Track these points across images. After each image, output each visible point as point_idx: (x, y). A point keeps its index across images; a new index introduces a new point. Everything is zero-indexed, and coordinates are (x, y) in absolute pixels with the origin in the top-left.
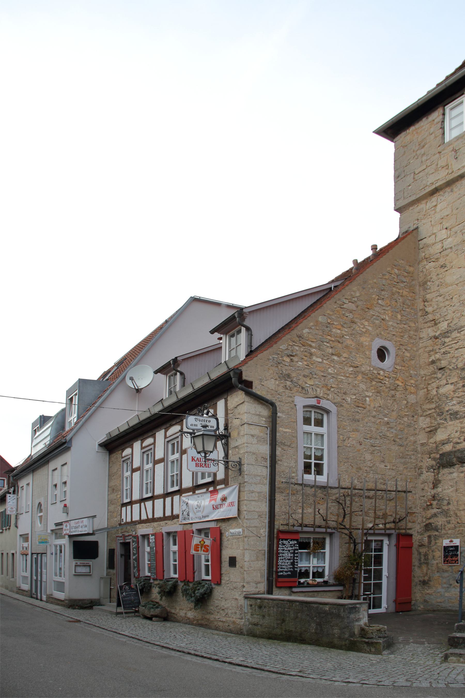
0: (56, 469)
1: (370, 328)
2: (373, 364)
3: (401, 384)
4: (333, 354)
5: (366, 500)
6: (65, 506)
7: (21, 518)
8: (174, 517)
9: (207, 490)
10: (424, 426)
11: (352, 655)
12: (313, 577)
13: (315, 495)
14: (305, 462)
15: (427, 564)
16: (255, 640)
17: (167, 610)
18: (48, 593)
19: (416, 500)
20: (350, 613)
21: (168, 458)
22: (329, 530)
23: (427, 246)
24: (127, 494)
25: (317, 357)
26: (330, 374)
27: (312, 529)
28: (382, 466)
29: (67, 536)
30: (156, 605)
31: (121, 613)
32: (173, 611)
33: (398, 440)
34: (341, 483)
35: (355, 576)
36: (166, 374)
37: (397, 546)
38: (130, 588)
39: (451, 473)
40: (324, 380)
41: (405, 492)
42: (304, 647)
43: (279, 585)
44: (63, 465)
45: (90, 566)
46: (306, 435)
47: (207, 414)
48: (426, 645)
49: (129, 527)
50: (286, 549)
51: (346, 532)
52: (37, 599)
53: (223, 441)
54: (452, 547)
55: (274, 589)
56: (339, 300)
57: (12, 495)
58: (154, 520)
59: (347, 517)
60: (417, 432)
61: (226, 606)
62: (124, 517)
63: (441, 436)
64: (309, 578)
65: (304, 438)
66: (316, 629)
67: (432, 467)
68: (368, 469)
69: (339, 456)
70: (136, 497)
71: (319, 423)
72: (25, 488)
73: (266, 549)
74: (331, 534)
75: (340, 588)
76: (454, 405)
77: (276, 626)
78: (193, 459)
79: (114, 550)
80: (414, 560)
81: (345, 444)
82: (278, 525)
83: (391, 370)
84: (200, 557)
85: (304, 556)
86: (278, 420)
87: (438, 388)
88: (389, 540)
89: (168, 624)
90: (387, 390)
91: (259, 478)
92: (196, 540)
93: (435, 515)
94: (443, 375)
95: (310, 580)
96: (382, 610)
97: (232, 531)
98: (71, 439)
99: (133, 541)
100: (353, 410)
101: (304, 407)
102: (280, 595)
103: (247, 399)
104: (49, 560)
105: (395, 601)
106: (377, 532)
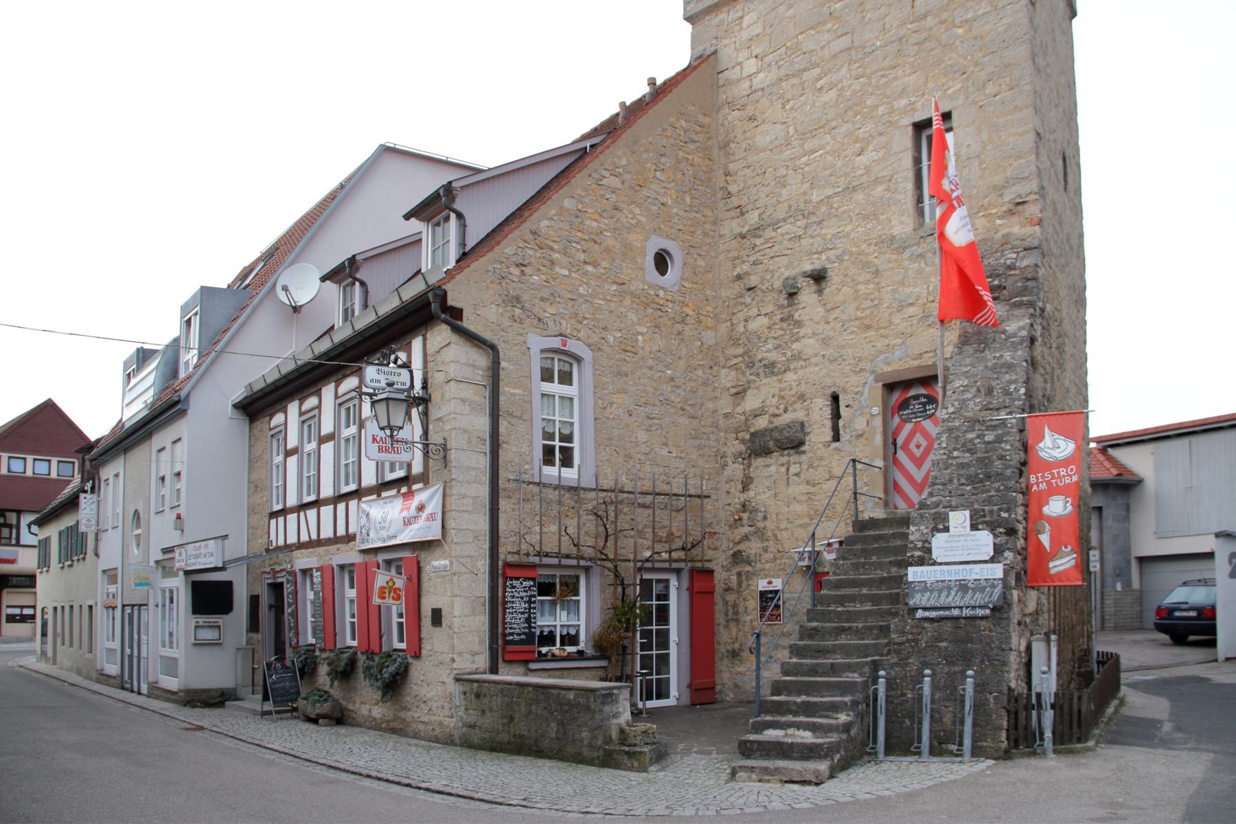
0: (163, 449)
1: (643, 219)
2: (648, 278)
3: (691, 313)
5: (640, 510)
6: (179, 517)
7: (104, 536)
8: (350, 538)
9: (399, 491)
10: (728, 385)
11: (607, 773)
12: (562, 644)
13: (560, 503)
14: (544, 446)
15: (737, 621)
16: (471, 752)
17: (341, 705)
18: (151, 679)
19: (718, 511)
20: (603, 703)
21: (331, 436)
22: (583, 563)
23: (730, 83)
24: (309, 485)
25: (562, 268)
27: (555, 561)
28: (664, 452)
29: (181, 573)
30: (325, 696)
31: (269, 713)
32: (350, 707)
33: (688, 408)
34: (600, 482)
35: (626, 642)
36: (339, 282)
37: (690, 589)
38: (284, 666)
40: (573, 306)
41: (699, 497)
42: (540, 762)
43: (507, 657)
44: (174, 442)
47: (395, 362)
48: (714, 755)
49: (281, 556)
50: (518, 593)
51: (610, 565)
52: (132, 691)
53: (420, 408)
54: (771, 592)
55: (501, 665)
56: (596, 171)
57: (88, 496)
58: (319, 543)
59: (611, 539)
60: (718, 394)
61: (428, 696)
62: (273, 537)
63: (751, 402)
64: (554, 645)
65: (546, 405)
66: (558, 731)
67: (741, 454)
68: (643, 458)
69: (596, 436)
70: (292, 501)
71: (566, 378)
72: (111, 481)
73: (487, 594)
74: (587, 569)
75: (603, 663)
77: (500, 727)
78: (374, 440)
79: (258, 597)
80: (717, 615)
81: (606, 414)
82: (506, 551)
83: (675, 289)
84: (389, 609)
85: (547, 607)
87: (746, 321)
88: (679, 580)
89: (343, 730)
90: (669, 323)
91: (473, 473)
92: (381, 579)
93: (746, 538)
94: (753, 299)
95: (556, 650)
96: (670, 702)
97: (435, 563)
98: (188, 395)
99: (288, 582)
100: (618, 356)
101: (542, 351)
102: (511, 675)
103: (454, 338)
104: (151, 617)
105: (690, 686)
106: (657, 565)
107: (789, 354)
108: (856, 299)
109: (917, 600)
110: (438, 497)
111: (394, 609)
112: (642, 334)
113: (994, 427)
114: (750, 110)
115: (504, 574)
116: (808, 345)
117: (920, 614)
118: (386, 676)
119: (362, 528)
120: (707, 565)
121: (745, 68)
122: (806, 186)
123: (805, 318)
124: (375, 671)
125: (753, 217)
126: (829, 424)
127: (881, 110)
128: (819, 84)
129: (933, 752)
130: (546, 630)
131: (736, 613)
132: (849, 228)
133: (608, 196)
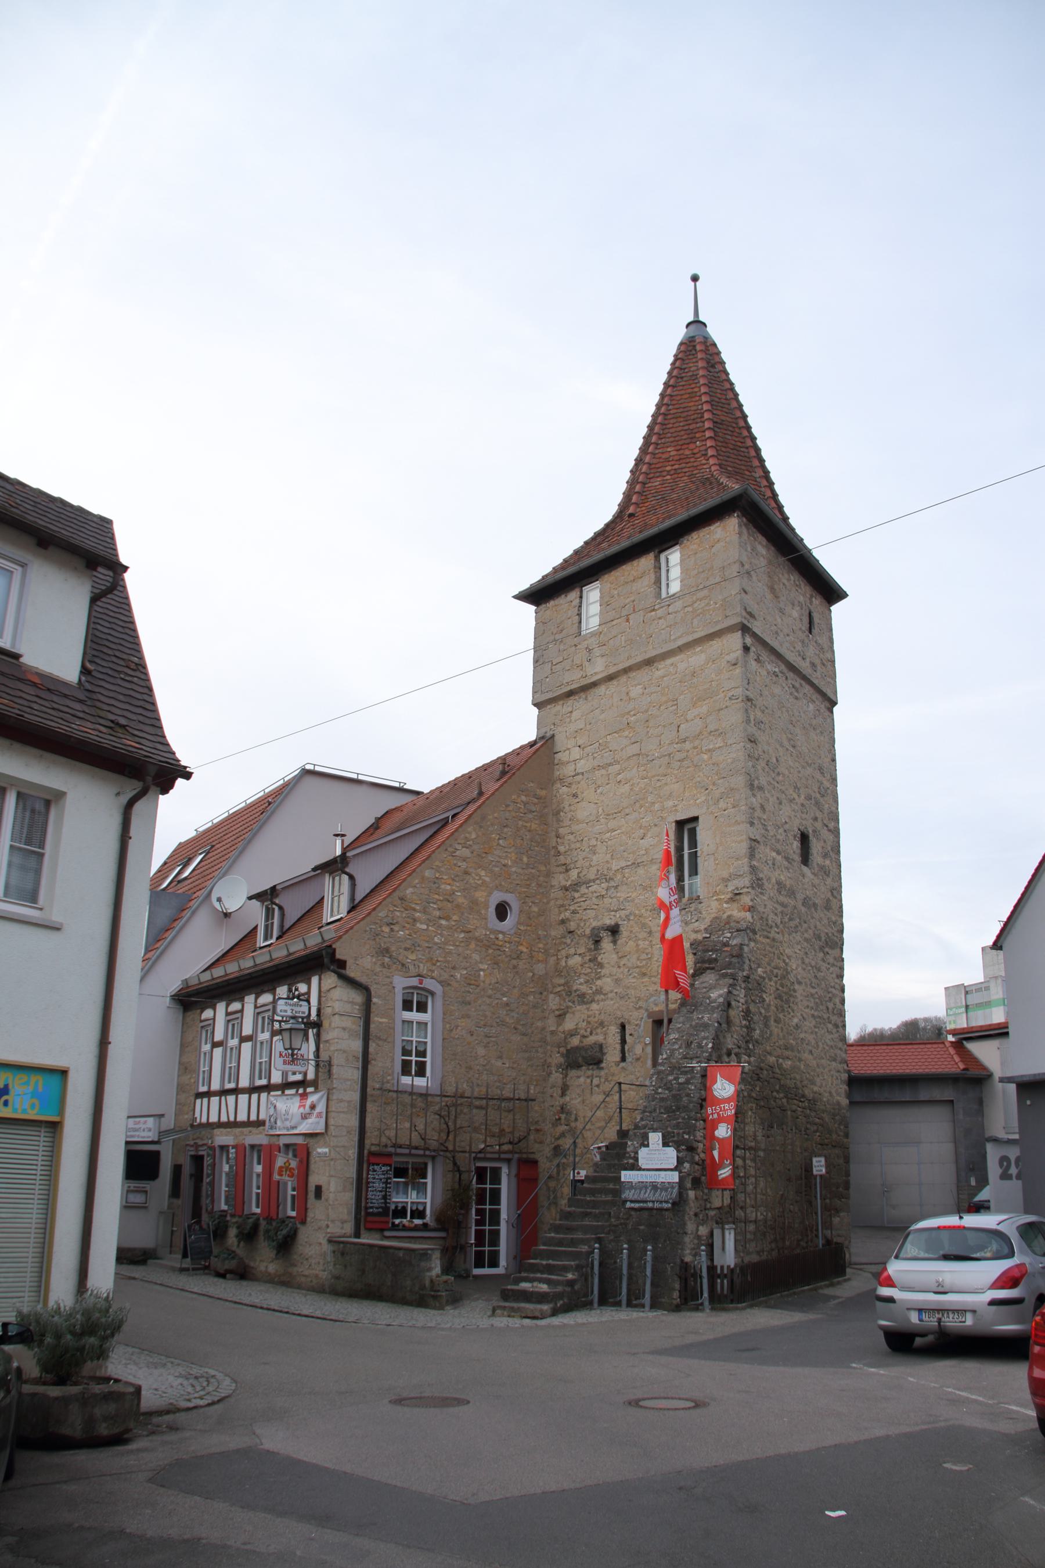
1: (487, 879)
2: (490, 926)
3: (525, 950)
4: (440, 918)
8: (259, 1123)
10: (554, 1008)
12: (412, 1217)
22: (427, 1153)
23: (562, 763)
24: (230, 1074)
26: (436, 944)
27: (407, 1151)
28: (499, 1063)
30: (232, 1255)
31: (187, 1270)
32: (252, 1264)
35: (461, 1218)
36: (263, 902)
37: (517, 1175)
38: (201, 1227)
39: (579, 1077)
45: (146, 1192)
46: (406, 1025)
50: (377, 1175)
55: (363, 1231)
56: (451, 846)
62: (197, 1115)
63: (569, 1024)
70: (215, 1086)
71: (422, 1008)
74: (433, 1158)
75: (443, 1234)
76: (581, 984)
78: (281, 1055)
82: (370, 1140)
83: (512, 932)
84: (286, 1184)
85: (401, 1187)
86: (373, 1008)
87: (567, 957)
88: (509, 1168)
89: (244, 1283)
92: (280, 1161)
93: (563, 1135)
96: (500, 1270)
97: (319, 1150)
99: (208, 1155)
101: (404, 989)
102: (367, 1239)
103: (340, 983)
106: (488, 1156)
107: (594, 988)
108: (637, 951)
109: (627, 1194)
110: (324, 1101)
111: (290, 1184)
112: (483, 970)
113: (686, 1073)
114: (574, 789)
115: (368, 1160)
116: (606, 983)
117: (628, 1205)
118: (280, 1237)
119: (270, 1117)
120: (532, 1156)
121: (572, 756)
122: (609, 856)
123: (605, 961)
124: (272, 1233)
125: (574, 874)
126: (618, 1047)
127: (657, 806)
128: (619, 777)
129: (629, 1304)
130: (400, 1206)
131: (555, 1198)
132: (634, 895)
133: (460, 864)
